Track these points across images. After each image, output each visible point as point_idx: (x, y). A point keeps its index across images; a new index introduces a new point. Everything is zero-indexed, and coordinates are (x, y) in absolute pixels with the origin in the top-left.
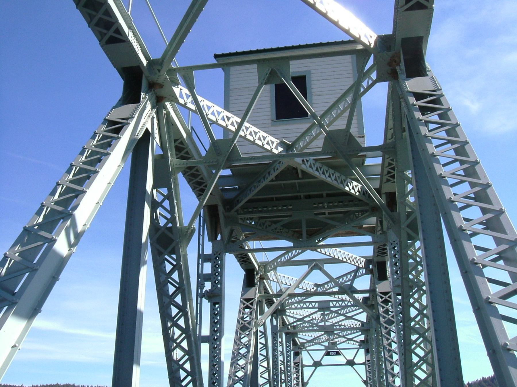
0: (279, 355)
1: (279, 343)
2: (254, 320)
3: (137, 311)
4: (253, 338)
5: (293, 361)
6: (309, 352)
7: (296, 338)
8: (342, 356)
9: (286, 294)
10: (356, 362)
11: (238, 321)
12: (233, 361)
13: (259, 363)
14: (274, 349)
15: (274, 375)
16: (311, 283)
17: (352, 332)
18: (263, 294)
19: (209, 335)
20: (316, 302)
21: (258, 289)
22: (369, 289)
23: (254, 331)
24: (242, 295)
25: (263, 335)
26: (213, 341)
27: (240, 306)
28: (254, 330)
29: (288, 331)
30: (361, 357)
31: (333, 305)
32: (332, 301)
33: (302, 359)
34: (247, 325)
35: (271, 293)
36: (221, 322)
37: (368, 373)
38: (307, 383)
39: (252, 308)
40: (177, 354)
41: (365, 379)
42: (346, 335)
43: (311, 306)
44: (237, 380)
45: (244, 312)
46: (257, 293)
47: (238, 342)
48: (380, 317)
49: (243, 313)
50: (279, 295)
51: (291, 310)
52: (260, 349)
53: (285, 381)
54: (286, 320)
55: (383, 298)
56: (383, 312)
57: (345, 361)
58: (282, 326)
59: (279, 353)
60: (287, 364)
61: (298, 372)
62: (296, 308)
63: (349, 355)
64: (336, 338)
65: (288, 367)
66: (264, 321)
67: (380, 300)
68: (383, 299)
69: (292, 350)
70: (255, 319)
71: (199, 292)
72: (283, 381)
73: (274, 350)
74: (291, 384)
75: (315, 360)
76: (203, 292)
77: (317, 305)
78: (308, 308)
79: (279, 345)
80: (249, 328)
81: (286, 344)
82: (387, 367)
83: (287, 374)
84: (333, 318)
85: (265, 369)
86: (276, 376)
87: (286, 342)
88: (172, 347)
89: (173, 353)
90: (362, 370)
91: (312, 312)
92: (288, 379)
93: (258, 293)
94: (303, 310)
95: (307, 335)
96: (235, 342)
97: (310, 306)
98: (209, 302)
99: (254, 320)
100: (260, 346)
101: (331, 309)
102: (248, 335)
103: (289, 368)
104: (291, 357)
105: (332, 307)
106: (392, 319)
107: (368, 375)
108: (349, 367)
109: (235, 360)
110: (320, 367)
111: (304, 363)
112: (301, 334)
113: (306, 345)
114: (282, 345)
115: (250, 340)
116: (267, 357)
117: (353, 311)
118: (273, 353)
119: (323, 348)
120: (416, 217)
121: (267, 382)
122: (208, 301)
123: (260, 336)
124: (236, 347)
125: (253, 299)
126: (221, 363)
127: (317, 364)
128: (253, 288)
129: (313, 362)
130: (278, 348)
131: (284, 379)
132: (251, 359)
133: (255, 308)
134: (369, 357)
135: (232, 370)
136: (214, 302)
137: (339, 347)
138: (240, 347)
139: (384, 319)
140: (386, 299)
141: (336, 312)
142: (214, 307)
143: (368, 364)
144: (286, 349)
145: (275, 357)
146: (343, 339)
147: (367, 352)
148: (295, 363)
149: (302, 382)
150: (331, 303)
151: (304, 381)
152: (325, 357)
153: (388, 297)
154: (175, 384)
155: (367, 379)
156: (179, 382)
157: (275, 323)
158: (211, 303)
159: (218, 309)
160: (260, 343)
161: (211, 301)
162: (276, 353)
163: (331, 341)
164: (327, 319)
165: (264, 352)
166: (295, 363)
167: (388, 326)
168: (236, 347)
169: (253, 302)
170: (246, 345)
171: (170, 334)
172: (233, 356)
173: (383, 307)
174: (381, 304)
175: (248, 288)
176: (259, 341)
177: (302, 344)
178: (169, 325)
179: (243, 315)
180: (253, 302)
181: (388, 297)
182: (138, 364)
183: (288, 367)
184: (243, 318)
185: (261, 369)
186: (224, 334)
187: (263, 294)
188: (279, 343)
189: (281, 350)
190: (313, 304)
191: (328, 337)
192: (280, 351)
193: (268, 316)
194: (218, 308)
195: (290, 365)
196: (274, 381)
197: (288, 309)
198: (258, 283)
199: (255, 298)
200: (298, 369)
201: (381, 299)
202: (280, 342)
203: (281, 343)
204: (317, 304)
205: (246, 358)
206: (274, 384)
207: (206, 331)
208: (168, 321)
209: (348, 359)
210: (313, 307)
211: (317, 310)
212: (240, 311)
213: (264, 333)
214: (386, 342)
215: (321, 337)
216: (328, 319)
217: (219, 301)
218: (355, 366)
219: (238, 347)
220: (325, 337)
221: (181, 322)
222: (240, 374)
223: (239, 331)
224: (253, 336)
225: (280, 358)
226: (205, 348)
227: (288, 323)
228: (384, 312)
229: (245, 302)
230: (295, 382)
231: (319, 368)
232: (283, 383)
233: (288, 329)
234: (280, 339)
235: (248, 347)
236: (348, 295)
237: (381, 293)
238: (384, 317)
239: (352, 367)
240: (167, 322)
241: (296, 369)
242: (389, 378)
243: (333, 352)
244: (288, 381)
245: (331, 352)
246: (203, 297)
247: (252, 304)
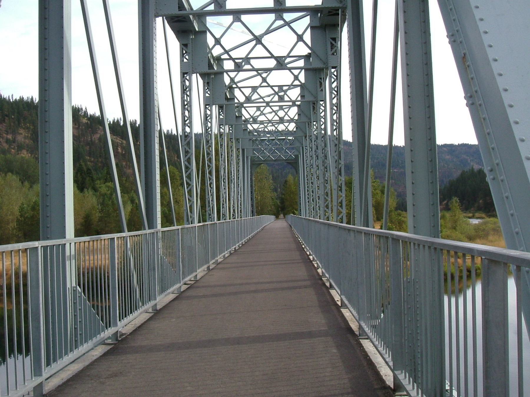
239: (312, 11)
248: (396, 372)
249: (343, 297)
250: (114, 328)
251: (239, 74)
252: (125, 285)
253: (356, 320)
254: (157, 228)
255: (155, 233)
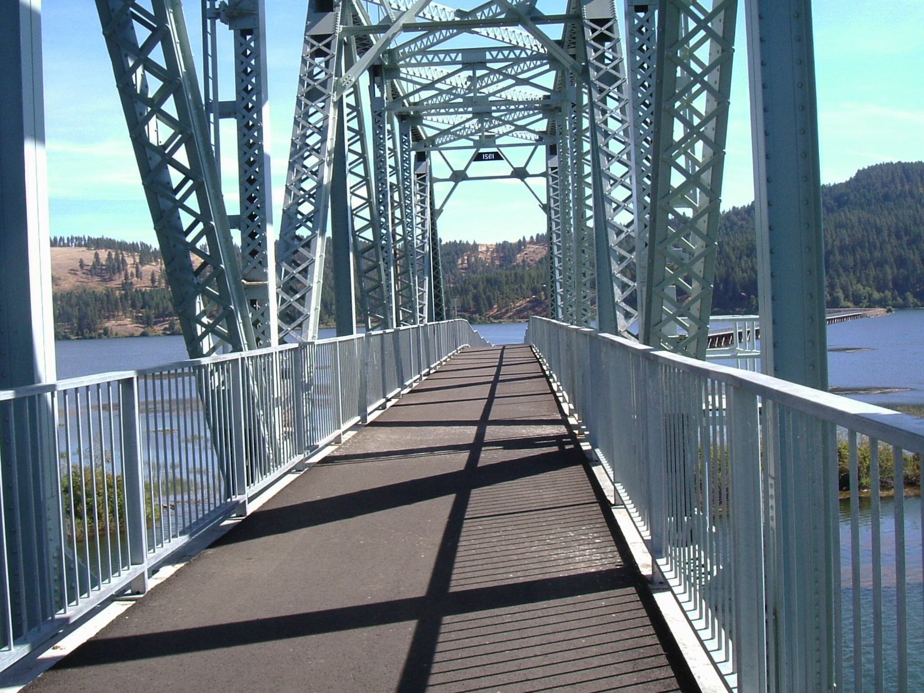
0: (387, 156)
1: (387, 134)
2: (334, 78)
3: (18, 10)
4: (333, 113)
5: (415, 171)
6: (442, 151)
7: (418, 127)
8: (505, 160)
9: (398, 25)
10: (531, 173)
11: (301, 81)
12: (293, 159)
13: (348, 167)
14: (379, 145)
15: (378, 192)
16: (448, 9)
17: (526, 114)
18: (352, 25)
19: (234, 99)
20: (457, 51)
21: (339, 15)
22: (564, 13)
23: (335, 100)
24: (308, 29)
25: (355, 114)
26: (244, 112)
27: (305, 50)
28: (335, 98)
29: (401, 109)
30: (539, 162)
31: (491, 58)
32: (490, 49)
33: (430, 166)
34: (319, 87)
35: (365, 24)
36: (259, 72)
37: (551, 190)
38: (441, 211)
39: (328, 54)
40: (157, 131)
41: (545, 202)
42: (514, 120)
43: (451, 55)
44: (303, 196)
45: (312, 62)
46: (339, 23)
47: (302, 122)
48: (590, 68)
49: (311, 65)
50: (384, 27)
51: (409, 69)
52: (349, 140)
53: (401, 222)
54: (397, 86)
55: (596, 30)
56: (596, 59)
57: (509, 171)
58: (392, 100)
59: (388, 152)
60: (403, 175)
61: (423, 191)
62: (419, 64)
63: (517, 157)
64: (495, 127)
65: (404, 180)
66: (353, 80)
67: (589, 35)
68: (596, 34)
69: (413, 150)
70: (336, 76)
71: (208, 6)
72: (397, 221)
73: (378, 146)
74: (412, 212)
75: (455, 169)
76: (217, 7)
77: (459, 58)
78: (442, 63)
79: (387, 137)
80: (324, 94)
81: (401, 139)
82: (601, 165)
83: (404, 193)
84: (490, 85)
85: (364, 201)
86: (383, 195)
87: (401, 134)
88: (141, 114)
89: (146, 127)
90: (540, 185)
91: (450, 72)
92: (405, 203)
93: (341, 24)
94: (433, 68)
95: (440, 120)
96: (296, 123)
97: (446, 60)
98: (230, 29)
99: (334, 78)
100: (348, 134)
101: (488, 65)
102: (323, 108)
103: (407, 192)
104: (410, 161)
105: (490, 61)
106: (614, 72)
107: (551, 194)
108: (517, 181)
109: (296, 157)
110: (464, 182)
111: (434, 175)
112: (429, 118)
113: (438, 141)
114: (393, 138)
115: (326, 118)
116: (363, 156)
117: (529, 69)
118: (375, 152)
119: (471, 143)
120: (562, 48)
121: (365, 204)
122: (228, 26)
123: (348, 115)
124: (298, 132)
125: (329, 35)
126: (265, 159)
127: (458, 177)
128: (331, 13)
129: (451, 172)
130: (384, 141)
131: (400, 217)
132: (330, 155)
133: (335, 53)
134: (555, 162)
135: (293, 178)
136: (243, 28)
137: (498, 142)
138: (308, 133)
139: (598, 72)
140: (602, 33)
141: (499, 71)
142: (244, 40)
143: (553, 175)
144: (402, 148)
145: (380, 160)
146: (508, 128)
147: (552, 151)
148: (418, 175)
149: (431, 209)
150: (487, 53)
151: (434, 206)
152: (474, 164)
153: (607, 29)
154: (159, 196)
155: (549, 200)
156: (170, 194)
157: (378, 94)
158: (235, 30)
159: (252, 44)
160: (350, 129)
161: (236, 26)
162: (382, 152)
163: (486, 134)
164: (478, 86)
165: (357, 147)
166: (418, 175)
167: (605, 87)
168: (298, 132)
169: (331, 41)
170: (319, 129)
171: (136, 85)
172: (293, 149)
173: (596, 50)
174: (592, 42)
175: (320, 14)
176: (346, 125)
177: (432, 140)
178: (131, 63)
179: (311, 68)
180: (331, 41)
181: (607, 29)
182: (40, 137)
183: (404, 180)
184: (311, 76)
185: (351, 180)
186: (266, 98)
187: (351, 25)
188: (387, 134)
189: (392, 147)
190: (453, 55)
191: (480, 125)
192: (389, 149)
193: (362, 70)
194: (250, 40)
195: (409, 178)
196: (379, 203)
197: (403, 66)
198: (341, 4)
199: (334, 34)
200: (423, 185)
201: (593, 33)
202: (388, 131)
203: (391, 132)
204: (460, 55)
205: (318, 153)
206: (379, 210)
207: (227, 92)
208: (126, 56)
209: (515, 166)
210: (454, 62)
211: (460, 66)
212: (304, 61)
213: (357, 108)
214: (601, 117)
215: (467, 125)
216: (482, 87)
217: (253, 27)
218: (527, 180)
219: (302, 132)
220: (474, 124)
221: (157, 55)
222: (309, 185)
223: (304, 101)
224: (332, 109)
225: (390, 162)
226: (228, 129)
227: (402, 95)
228: (596, 59)
229: (315, 43)
230: (419, 208)
231: (462, 184)
232: (398, 224)
233: (404, 105)
234: (389, 125)
235: (322, 131)
236: (525, 26)
237: (592, 21)
238: (598, 69)
239: (523, 180)
240: (124, 59)
241: (420, 185)
242: (604, 186)
243: (488, 153)
244: (406, 207)
245: (485, 153)
246: (217, 19)
247: (328, 46)
248: (616, 485)
249: (619, 486)
250: (18, 648)
251: (458, 186)
252: (255, 437)
253: (611, 480)
254: (40, 382)
255: (37, 397)
